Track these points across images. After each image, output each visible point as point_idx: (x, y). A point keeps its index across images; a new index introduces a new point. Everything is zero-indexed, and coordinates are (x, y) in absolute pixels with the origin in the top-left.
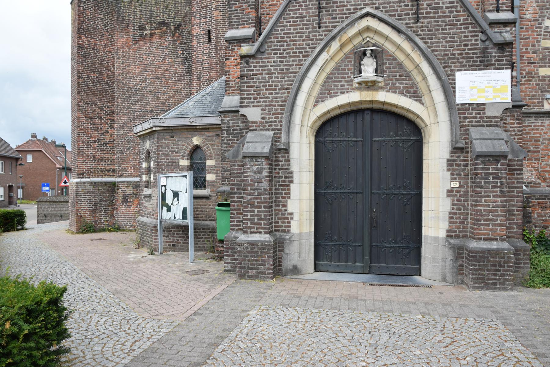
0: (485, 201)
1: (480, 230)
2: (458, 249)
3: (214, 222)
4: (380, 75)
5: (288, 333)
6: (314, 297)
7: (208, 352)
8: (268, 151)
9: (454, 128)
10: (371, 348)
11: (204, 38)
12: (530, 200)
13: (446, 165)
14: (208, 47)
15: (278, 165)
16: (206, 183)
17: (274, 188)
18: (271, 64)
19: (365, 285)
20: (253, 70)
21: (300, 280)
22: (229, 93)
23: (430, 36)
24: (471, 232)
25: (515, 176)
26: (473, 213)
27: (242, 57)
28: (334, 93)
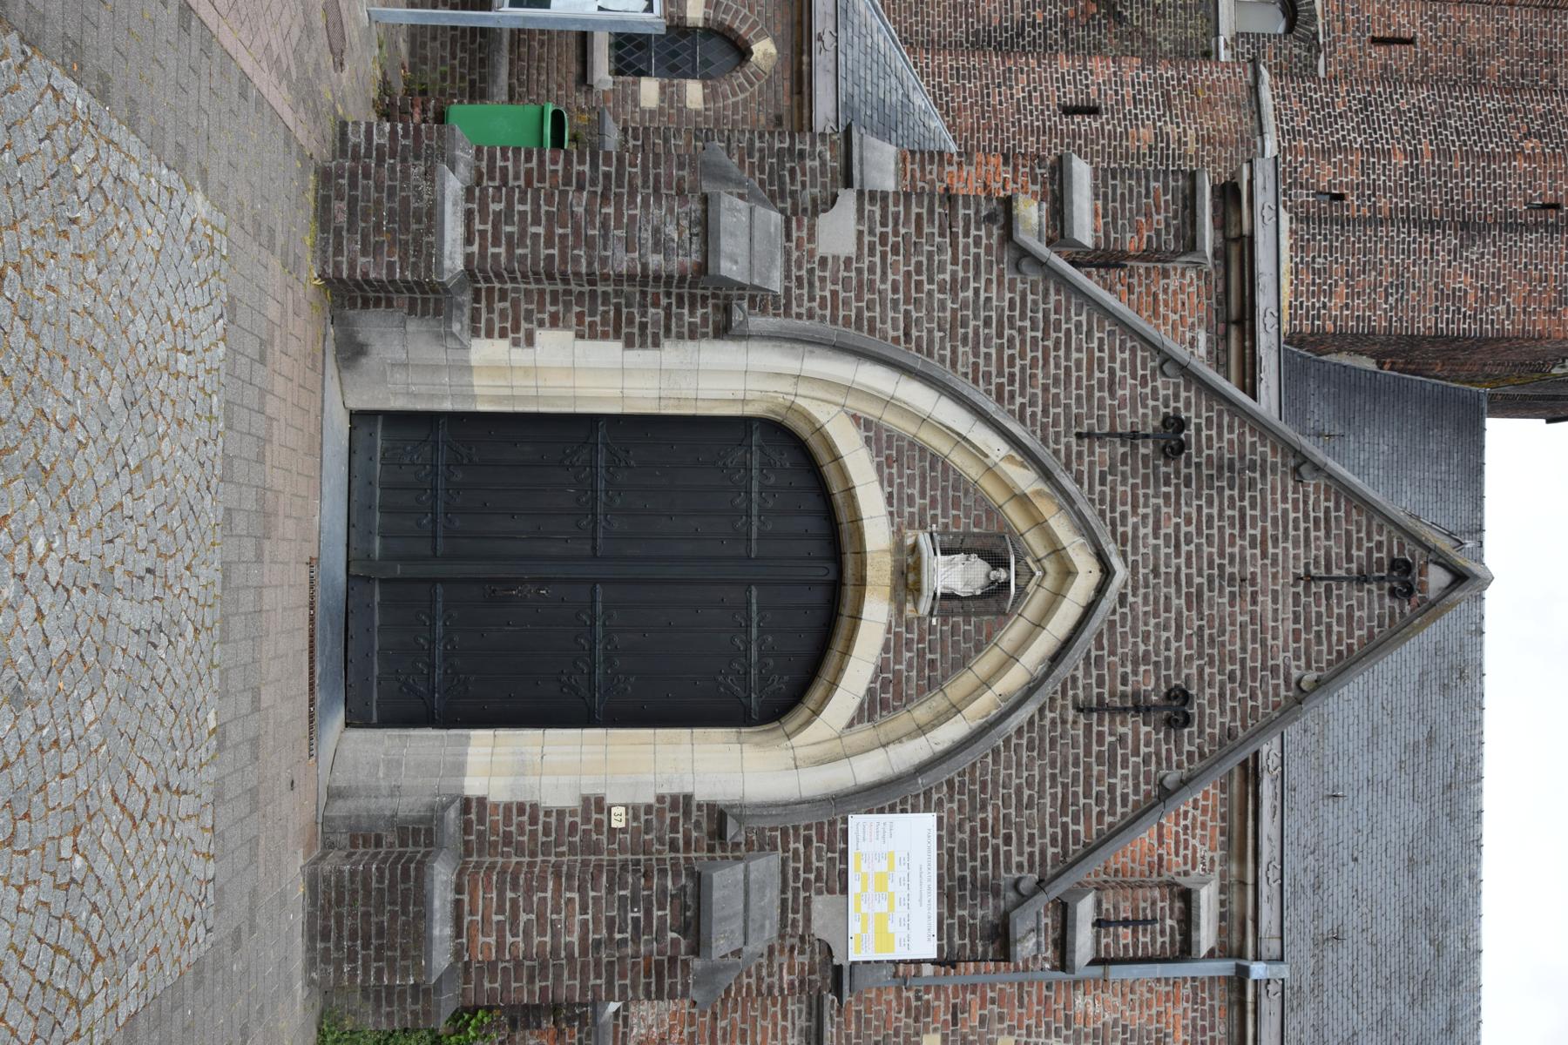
0: (570, 900)
1: (487, 889)
2: (429, 832)
3: (505, 98)
4: (937, 605)
5: (135, 313)
6: (262, 403)
7: (48, 43)
8: (723, 273)
9: (779, 810)
10: (95, 571)
11: (1076, 94)
12: (577, 1023)
13: (676, 790)
14: (1048, 106)
15: (680, 304)
16: (630, 79)
17: (610, 289)
18: (982, 291)
19: (310, 564)
20: (966, 235)
21: (319, 365)
22: (904, 160)
23: (1037, 742)
24: (478, 865)
25: (642, 980)
26: (536, 870)
27: (1008, 203)
28: (891, 474)
